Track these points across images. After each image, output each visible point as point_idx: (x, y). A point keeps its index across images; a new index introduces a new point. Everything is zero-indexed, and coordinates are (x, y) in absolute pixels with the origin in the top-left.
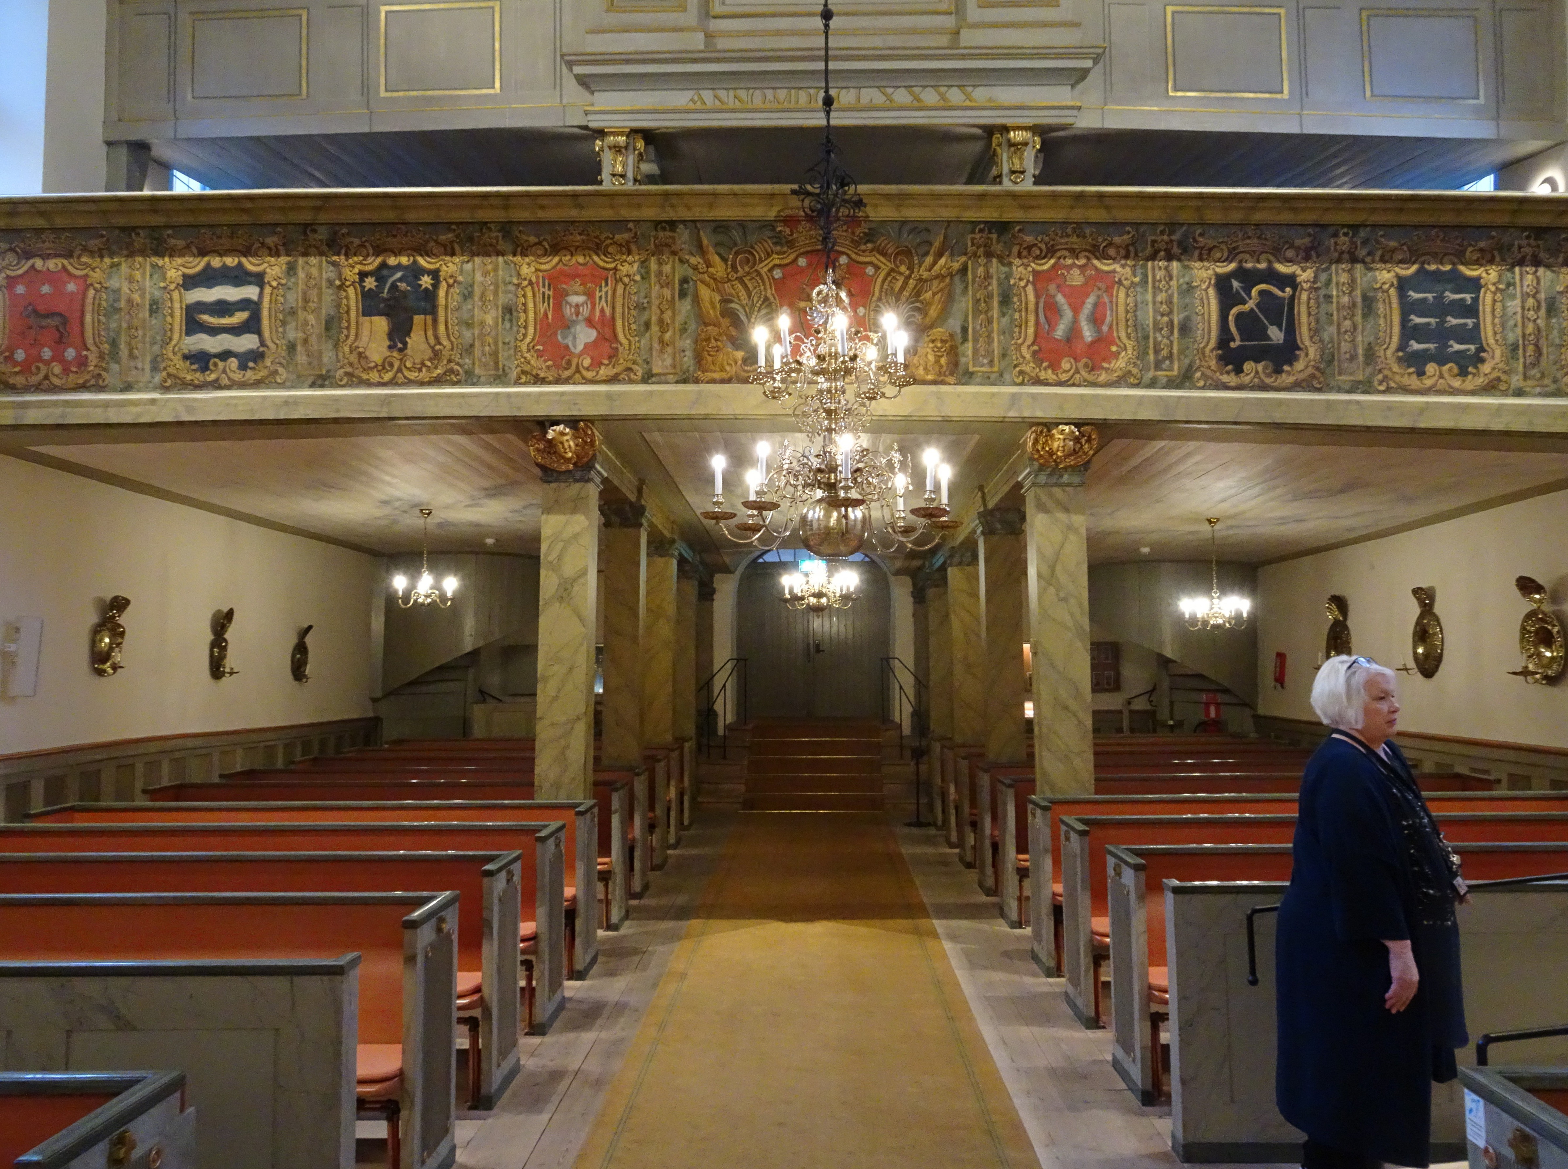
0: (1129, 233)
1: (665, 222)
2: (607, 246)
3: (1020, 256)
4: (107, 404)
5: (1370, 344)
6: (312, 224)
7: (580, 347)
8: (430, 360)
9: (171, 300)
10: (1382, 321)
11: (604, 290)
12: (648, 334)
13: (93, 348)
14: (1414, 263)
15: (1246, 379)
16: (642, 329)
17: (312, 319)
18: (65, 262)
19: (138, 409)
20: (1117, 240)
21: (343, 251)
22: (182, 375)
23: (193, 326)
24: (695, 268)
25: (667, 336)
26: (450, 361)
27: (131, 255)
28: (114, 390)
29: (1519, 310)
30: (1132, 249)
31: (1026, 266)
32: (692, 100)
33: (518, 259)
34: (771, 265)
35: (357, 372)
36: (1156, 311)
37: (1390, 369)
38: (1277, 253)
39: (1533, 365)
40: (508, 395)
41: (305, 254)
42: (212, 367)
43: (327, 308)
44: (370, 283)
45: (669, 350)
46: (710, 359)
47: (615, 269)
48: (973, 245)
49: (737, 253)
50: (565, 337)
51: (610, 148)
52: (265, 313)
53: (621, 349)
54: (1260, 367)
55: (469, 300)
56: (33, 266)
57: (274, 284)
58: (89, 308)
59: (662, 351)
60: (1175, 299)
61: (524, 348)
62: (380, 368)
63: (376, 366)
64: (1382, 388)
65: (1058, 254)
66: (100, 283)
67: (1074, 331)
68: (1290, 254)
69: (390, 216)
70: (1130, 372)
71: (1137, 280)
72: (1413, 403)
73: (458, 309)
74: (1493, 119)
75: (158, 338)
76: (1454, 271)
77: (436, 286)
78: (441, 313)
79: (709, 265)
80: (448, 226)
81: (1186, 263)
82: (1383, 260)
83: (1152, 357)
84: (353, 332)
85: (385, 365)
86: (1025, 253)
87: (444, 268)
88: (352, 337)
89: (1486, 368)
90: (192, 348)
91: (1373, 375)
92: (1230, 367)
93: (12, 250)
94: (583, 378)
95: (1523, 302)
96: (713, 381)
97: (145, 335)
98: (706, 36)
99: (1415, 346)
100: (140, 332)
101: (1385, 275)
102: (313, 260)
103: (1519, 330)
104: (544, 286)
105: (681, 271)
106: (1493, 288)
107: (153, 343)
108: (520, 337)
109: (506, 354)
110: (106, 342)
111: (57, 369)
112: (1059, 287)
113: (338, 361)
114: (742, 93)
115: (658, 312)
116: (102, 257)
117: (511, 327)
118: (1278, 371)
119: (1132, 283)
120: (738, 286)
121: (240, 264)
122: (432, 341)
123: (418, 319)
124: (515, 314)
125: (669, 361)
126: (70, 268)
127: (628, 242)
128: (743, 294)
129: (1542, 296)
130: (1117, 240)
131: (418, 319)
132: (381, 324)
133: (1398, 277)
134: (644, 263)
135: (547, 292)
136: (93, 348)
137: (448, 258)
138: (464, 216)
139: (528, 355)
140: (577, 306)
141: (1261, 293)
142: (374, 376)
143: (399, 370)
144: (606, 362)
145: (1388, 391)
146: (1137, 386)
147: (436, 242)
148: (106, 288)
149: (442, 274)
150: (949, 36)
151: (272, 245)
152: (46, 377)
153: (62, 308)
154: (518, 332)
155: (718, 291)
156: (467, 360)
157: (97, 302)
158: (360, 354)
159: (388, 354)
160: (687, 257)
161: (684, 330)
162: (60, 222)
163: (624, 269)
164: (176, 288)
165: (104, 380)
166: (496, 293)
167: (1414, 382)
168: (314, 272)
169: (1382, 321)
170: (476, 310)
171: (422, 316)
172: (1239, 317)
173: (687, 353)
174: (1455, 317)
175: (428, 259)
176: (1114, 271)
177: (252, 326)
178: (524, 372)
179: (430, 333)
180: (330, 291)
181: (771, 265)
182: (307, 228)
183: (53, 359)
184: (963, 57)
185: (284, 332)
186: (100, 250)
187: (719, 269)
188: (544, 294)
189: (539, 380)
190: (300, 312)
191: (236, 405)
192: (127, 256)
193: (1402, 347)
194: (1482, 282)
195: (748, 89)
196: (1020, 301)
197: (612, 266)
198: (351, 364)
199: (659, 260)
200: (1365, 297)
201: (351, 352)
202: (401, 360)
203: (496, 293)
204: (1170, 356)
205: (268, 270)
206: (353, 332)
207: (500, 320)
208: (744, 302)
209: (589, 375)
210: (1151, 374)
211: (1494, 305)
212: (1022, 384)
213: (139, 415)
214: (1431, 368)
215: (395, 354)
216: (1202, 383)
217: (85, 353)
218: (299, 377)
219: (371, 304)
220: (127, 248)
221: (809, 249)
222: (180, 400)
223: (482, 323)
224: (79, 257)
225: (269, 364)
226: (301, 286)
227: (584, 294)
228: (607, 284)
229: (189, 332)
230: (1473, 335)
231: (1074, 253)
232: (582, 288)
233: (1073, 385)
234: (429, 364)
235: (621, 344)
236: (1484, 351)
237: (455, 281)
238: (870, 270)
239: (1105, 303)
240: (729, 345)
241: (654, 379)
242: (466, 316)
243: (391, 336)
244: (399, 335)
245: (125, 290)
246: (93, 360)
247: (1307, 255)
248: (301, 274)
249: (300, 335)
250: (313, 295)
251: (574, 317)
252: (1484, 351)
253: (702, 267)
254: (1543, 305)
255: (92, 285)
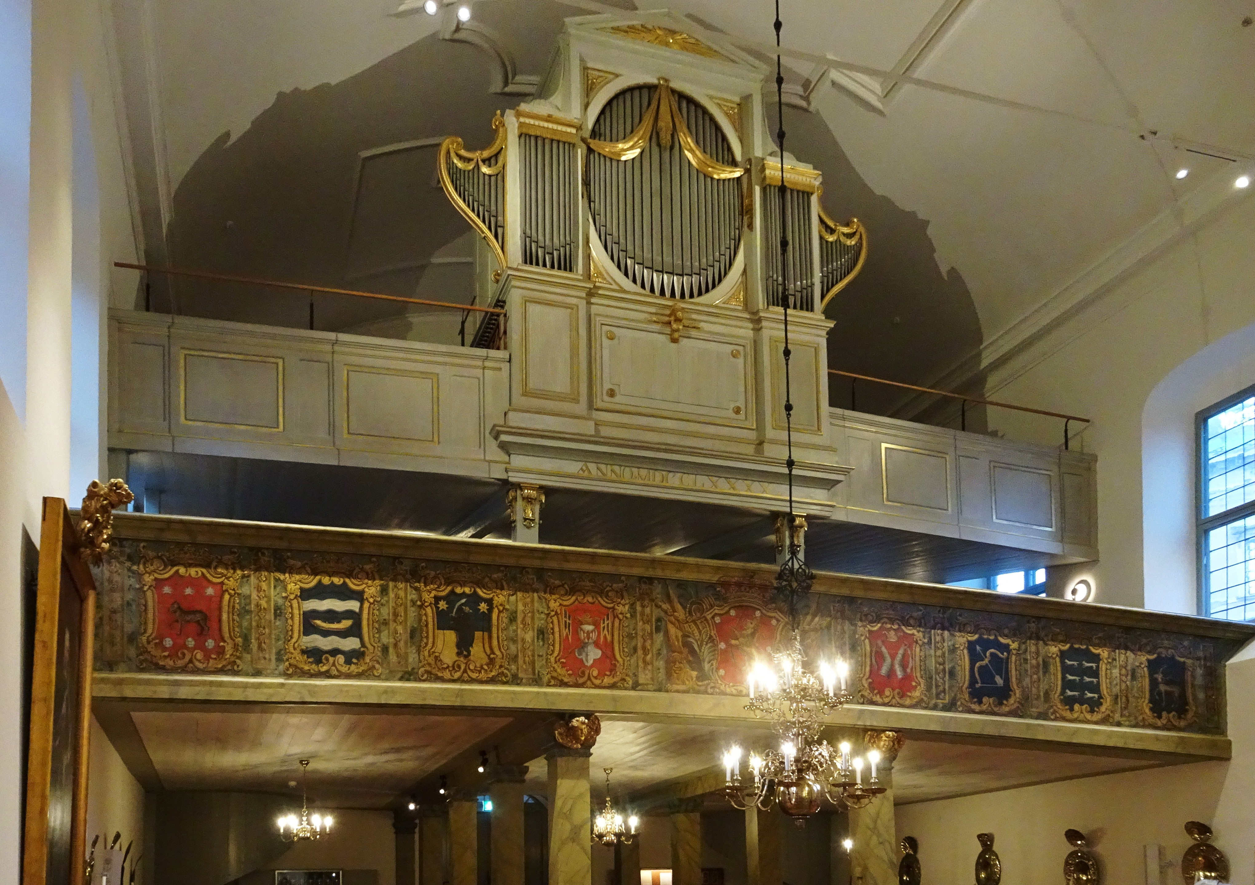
0: (921, 610)
1: (647, 578)
2: (608, 592)
3: (861, 620)
4: (245, 686)
5: (1046, 690)
6: (399, 558)
7: (591, 662)
8: (487, 665)
9: (291, 606)
10: (1052, 677)
11: (606, 622)
12: (635, 656)
13: (229, 641)
14: (1068, 643)
15: (984, 707)
16: (632, 651)
17: (400, 629)
18: (204, 571)
19: (270, 691)
20: (915, 614)
21: (423, 580)
22: (301, 666)
23: (309, 628)
24: (666, 612)
25: (649, 657)
26: (501, 667)
27: (258, 569)
28: (247, 675)
29: (1118, 675)
30: (923, 621)
31: (865, 626)
32: (582, 469)
33: (547, 596)
34: (713, 614)
35: (434, 671)
36: (936, 662)
37: (1056, 706)
38: (999, 630)
39: (1126, 708)
40: (545, 693)
41: (394, 580)
42: (324, 661)
43: (411, 621)
44: (443, 605)
45: (650, 667)
46: (675, 675)
47: (613, 608)
48: (834, 610)
49: (692, 604)
50: (580, 654)
51: (524, 499)
52: (365, 623)
53: (618, 665)
54: (991, 700)
55: (514, 623)
56: (177, 571)
57: (371, 600)
58: (225, 608)
59: (645, 668)
60: (946, 655)
61: (553, 660)
62: (451, 669)
63: (448, 667)
64: (1052, 717)
65: (882, 621)
66: (234, 590)
67: (891, 672)
68: (1006, 631)
69: (458, 557)
70: (922, 699)
71: (926, 641)
72: (1069, 727)
73: (506, 629)
74: (1059, 541)
75: (282, 636)
76: (1087, 649)
77: (490, 610)
78: (494, 630)
79: (674, 611)
80: (498, 568)
81: (952, 632)
82: (1053, 640)
83: (934, 690)
84: (431, 640)
85: (455, 667)
86: (863, 618)
87: (496, 598)
88: (430, 645)
89: (1103, 709)
90: (309, 645)
91: (1049, 709)
92: (975, 700)
93: (159, 558)
94: (593, 684)
95: (1120, 670)
96: (678, 691)
97: (270, 634)
98: (596, 424)
99: (1069, 693)
100: (267, 630)
101: (1054, 649)
102: (401, 585)
103: (1118, 687)
104: (565, 617)
105: (657, 613)
106: (1106, 661)
107: (278, 640)
108: (550, 652)
109: (540, 664)
110: (240, 636)
111: (199, 655)
112: (883, 642)
113: (420, 661)
114: (616, 468)
115: (642, 640)
116: (234, 570)
117: (543, 645)
118: (1001, 704)
119: (924, 643)
120: (693, 625)
121: (345, 583)
122: (488, 652)
123: (478, 634)
124: (546, 635)
125: (649, 676)
126: (208, 575)
127: (621, 590)
128: (696, 633)
129: (1129, 668)
130: (915, 614)
131: (478, 634)
132: (451, 636)
133: (1060, 651)
134: (632, 605)
135: (568, 621)
136: (229, 641)
137: (498, 591)
138: (511, 562)
139: (555, 666)
140: (588, 633)
141: (992, 654)
142: (447, 675)
143: (465, 671)
144: (608, 673)
145: (1056, 719)
146: (925, 708)
147: (490, 578)
148: (239, 594)
149: (495, 602)
150: (754, 446)
151: (369, 571)
152: (191, 661)
153: (201, 606)
154: (548, 648)
155: (681, 629)
156: (513, 666)
157: (231, 604)
158: (436, 658)
159: (457, 659)
160: (660, 603)
161: (659, 654)
162: (200, 539)
163: (620, 608)
164: (295, 598)
165: (238, 666)
166: (533, 618)
167: (1068, 714)
168: (402, 594)
169: (1052, 677)
170: (519, 631)
171: (481, 633)
172: (981, 667)
173: (661, 670)
174: (1088, 677)
175: (485, 591)
176: (913, 635)
177: (355, 631)
178: (552, 677)
179: (487, 646)
180: (413, 609)
181: (715, 614)
182: (396, 560)
183: (195, 648)
184: (767, 463)
185: (379, 638)
186: (233, 564)
187: (681, 614)
188: (566, 622)
189: (563, 684)
190: (391, 622)
191: (347, 691)
192: (256, 570)
193: (1063, 692)
194: (1101, 657)
195: (621, 466)
196: (862, 649)
197: (611, 605)
198: (429, 664)
199: (642, 604)
200: (1043, 661)
201: (429, 656)
202: (466, 663)
203: (533, 618)
204: (944, 691)
205: (366, 590)
206: (431, 640)
207: (536, 640)
208: (697, 638)
209: (597, 682)
210: (933, 702)
211: (1106, 671)
212: (863, 703)
213: (272, 695)
214: (1077, 707)
215: (462, 659)
216: (960, 709)
217: (222, 644)
218: (391, 672)
219: (444, 621)
220: (255, 564)
221: (737, 604)
222: (305, 686)
223: (523, 640)
224: (215, 568)
225: (368, 661)
226: (392, 604)
227: (594, 625)
228: (608, 619)
229: (306, 633)
230: (1096, 688)
231: (892, 621)
232: (590, 620)
233: (891, 706)
234: (486, 667)
235: (618, 661)
236: (1102, 698)
237: (504, 608)
238: (774, 622)
239: (908, 655)
240: (688, 666)
241: (639, 687)
242: (511, 634)
243: (458, 646)
244: (464, 646)
245: (254, 595)
246: (229, 650)
247: (1014, 634)
248: (392, 595)
249: (392, 640)
250: (401, 610)
251: (586, 641)
252: (1102, 698)
253: (670, 611)
254: (1130, 673)
255: (227, 590)
